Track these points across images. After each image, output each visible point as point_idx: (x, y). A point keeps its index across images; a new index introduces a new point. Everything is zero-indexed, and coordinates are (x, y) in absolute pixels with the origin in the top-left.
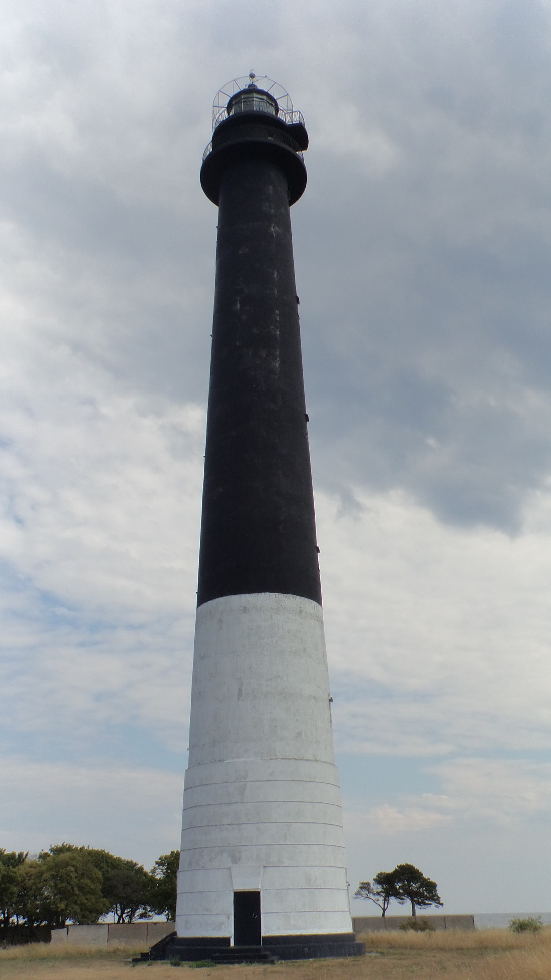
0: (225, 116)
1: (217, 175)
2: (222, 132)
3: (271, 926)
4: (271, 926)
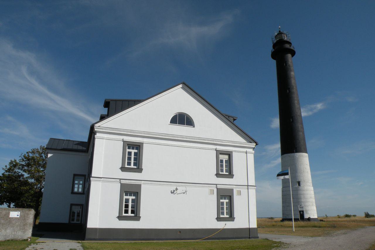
0: (275, 41)
1: (274, 56)
2: (274, 46)
3: (306, 216)
4: (306, 216)
